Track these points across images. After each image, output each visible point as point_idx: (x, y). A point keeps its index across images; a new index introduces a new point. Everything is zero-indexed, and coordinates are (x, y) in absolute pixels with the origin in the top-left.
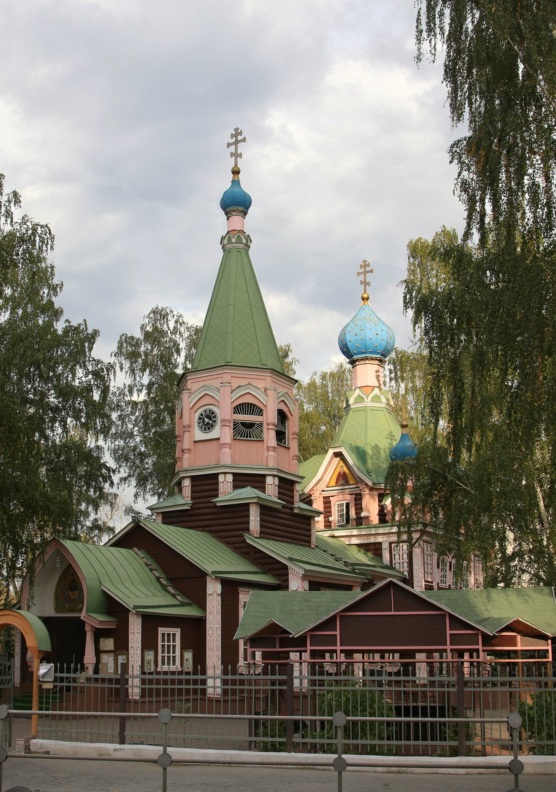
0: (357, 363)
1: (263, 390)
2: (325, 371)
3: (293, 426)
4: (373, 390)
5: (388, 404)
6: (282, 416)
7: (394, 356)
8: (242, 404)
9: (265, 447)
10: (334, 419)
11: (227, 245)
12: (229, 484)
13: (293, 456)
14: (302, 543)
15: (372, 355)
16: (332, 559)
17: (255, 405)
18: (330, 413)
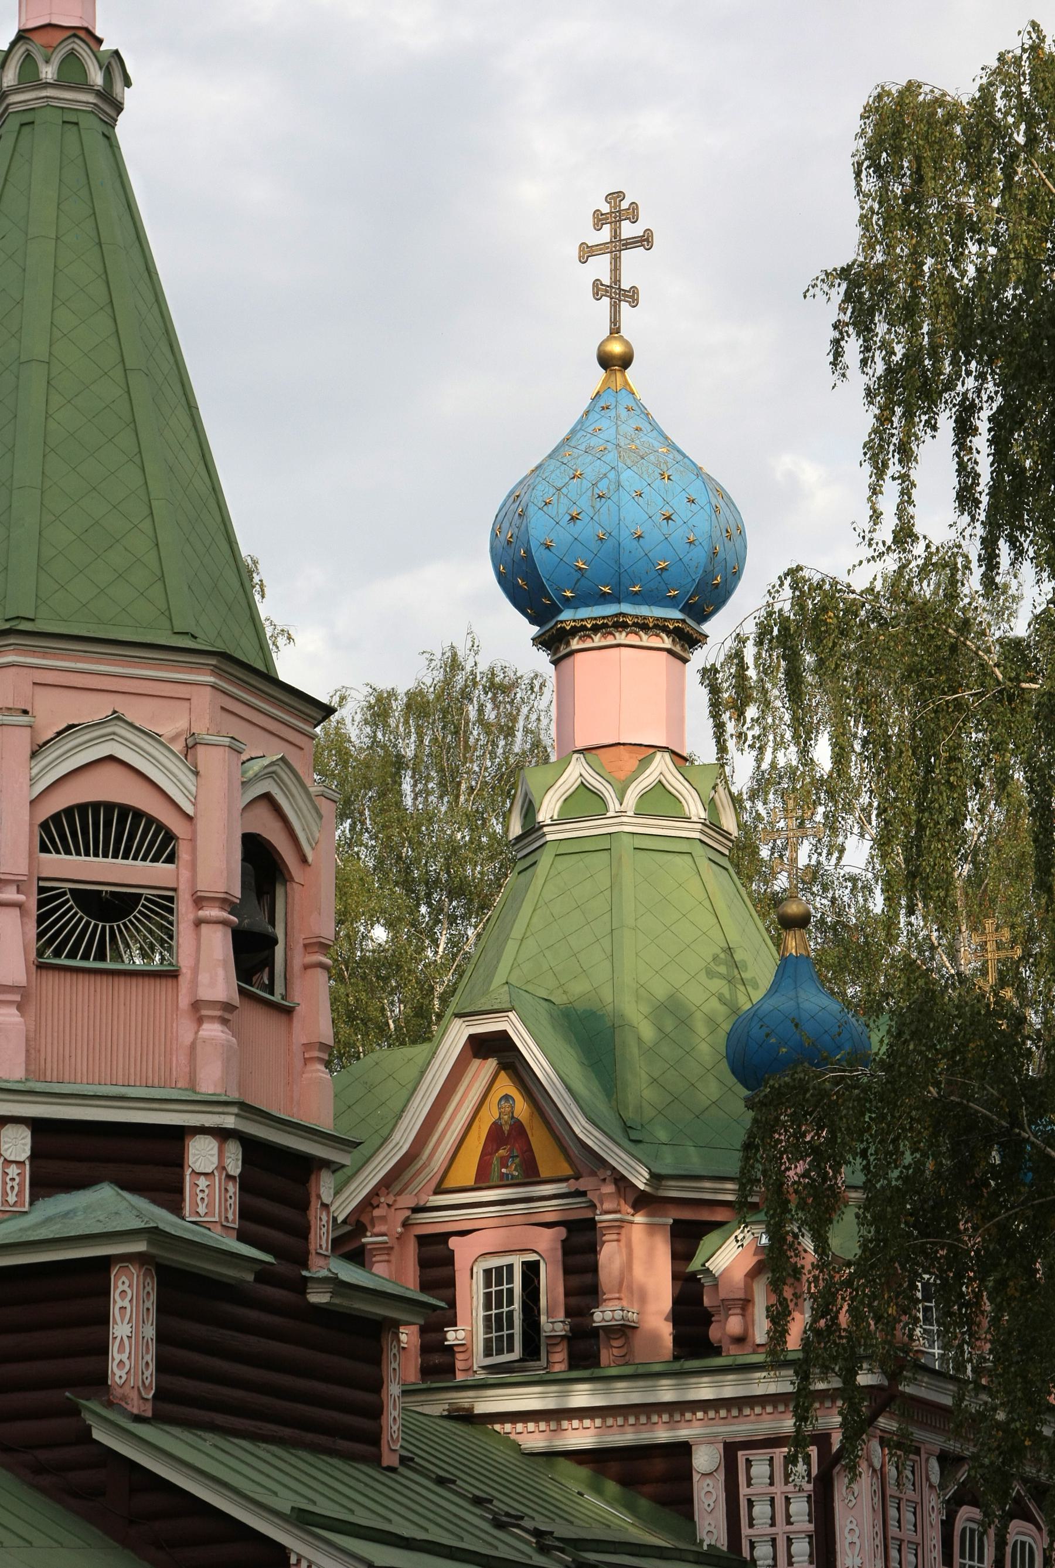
0: (575, 644)
1: (178, 747)
2: (384, 685)
3: (309, 910)
4: (645, 763)
5: (713, 825)
6: (263, 866)
7: (787, 606)
8: (82, 808)
9: (184, 1002)
10: (429, 895)
11: (16, 90)
12: (13, 1171)
13: (307, 1046)
14: (343, 1444)
15: (644, 611)
16: (475, 1518)
17: (138, 814)
18: (408, 871)
